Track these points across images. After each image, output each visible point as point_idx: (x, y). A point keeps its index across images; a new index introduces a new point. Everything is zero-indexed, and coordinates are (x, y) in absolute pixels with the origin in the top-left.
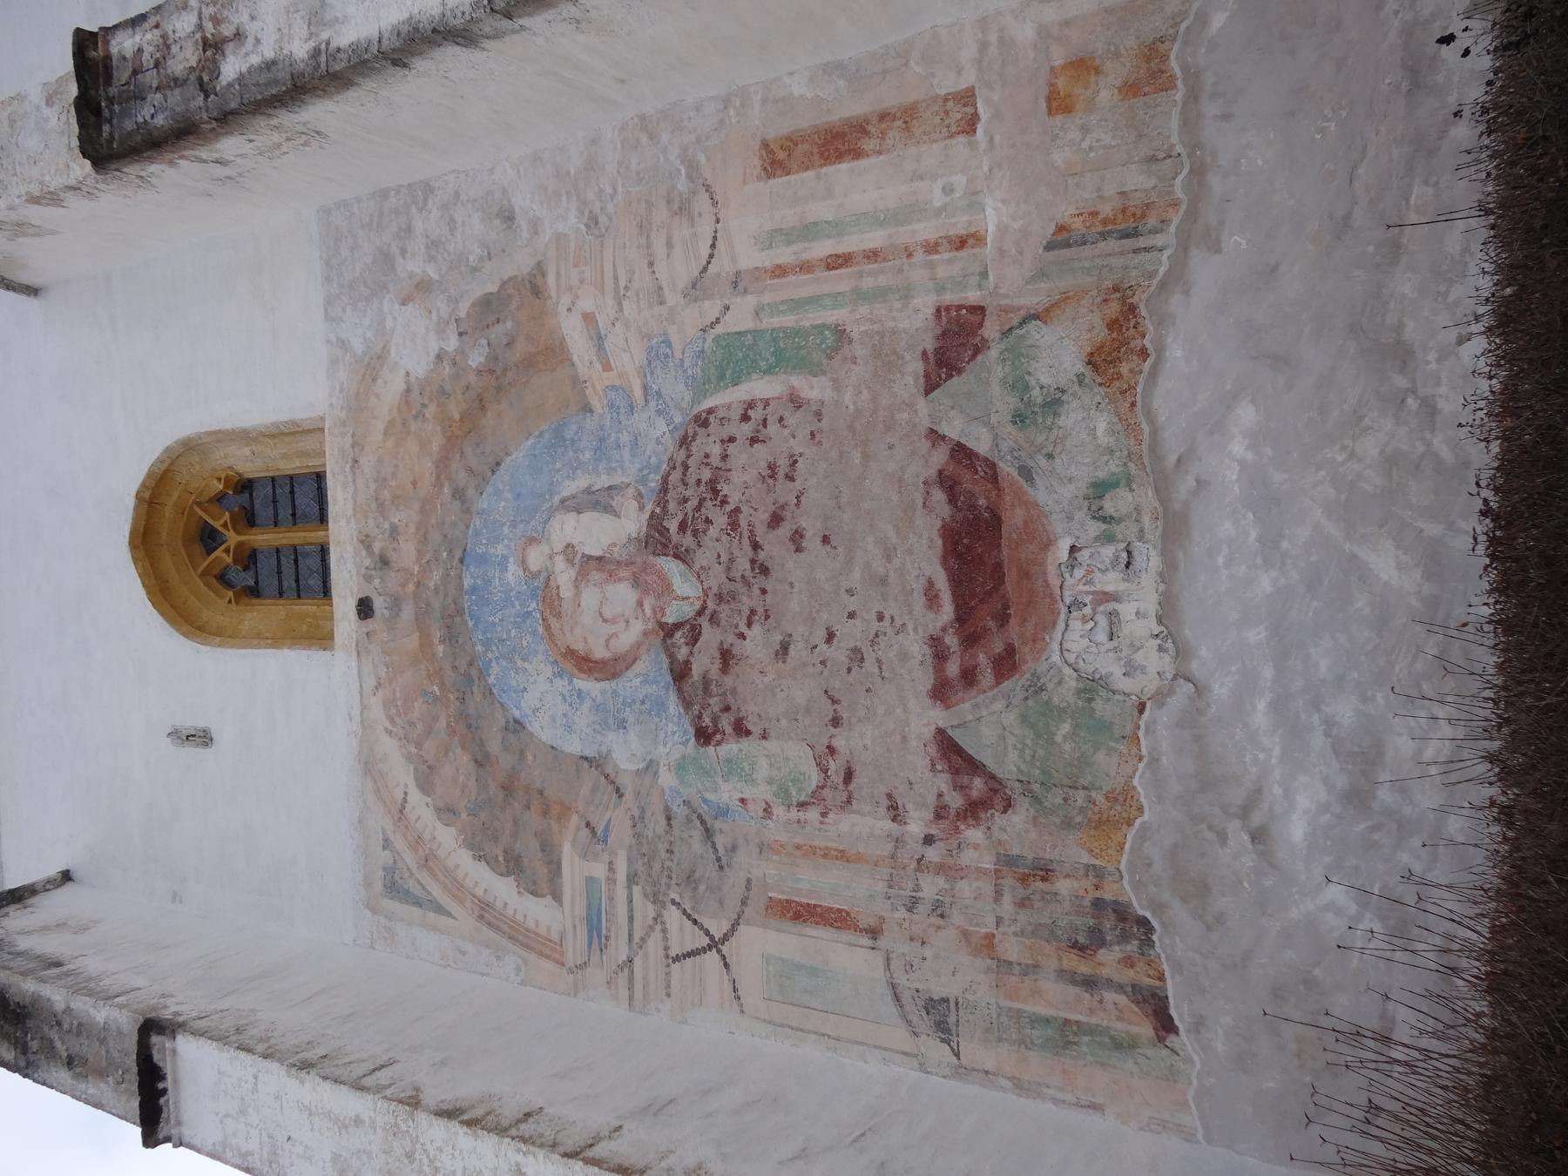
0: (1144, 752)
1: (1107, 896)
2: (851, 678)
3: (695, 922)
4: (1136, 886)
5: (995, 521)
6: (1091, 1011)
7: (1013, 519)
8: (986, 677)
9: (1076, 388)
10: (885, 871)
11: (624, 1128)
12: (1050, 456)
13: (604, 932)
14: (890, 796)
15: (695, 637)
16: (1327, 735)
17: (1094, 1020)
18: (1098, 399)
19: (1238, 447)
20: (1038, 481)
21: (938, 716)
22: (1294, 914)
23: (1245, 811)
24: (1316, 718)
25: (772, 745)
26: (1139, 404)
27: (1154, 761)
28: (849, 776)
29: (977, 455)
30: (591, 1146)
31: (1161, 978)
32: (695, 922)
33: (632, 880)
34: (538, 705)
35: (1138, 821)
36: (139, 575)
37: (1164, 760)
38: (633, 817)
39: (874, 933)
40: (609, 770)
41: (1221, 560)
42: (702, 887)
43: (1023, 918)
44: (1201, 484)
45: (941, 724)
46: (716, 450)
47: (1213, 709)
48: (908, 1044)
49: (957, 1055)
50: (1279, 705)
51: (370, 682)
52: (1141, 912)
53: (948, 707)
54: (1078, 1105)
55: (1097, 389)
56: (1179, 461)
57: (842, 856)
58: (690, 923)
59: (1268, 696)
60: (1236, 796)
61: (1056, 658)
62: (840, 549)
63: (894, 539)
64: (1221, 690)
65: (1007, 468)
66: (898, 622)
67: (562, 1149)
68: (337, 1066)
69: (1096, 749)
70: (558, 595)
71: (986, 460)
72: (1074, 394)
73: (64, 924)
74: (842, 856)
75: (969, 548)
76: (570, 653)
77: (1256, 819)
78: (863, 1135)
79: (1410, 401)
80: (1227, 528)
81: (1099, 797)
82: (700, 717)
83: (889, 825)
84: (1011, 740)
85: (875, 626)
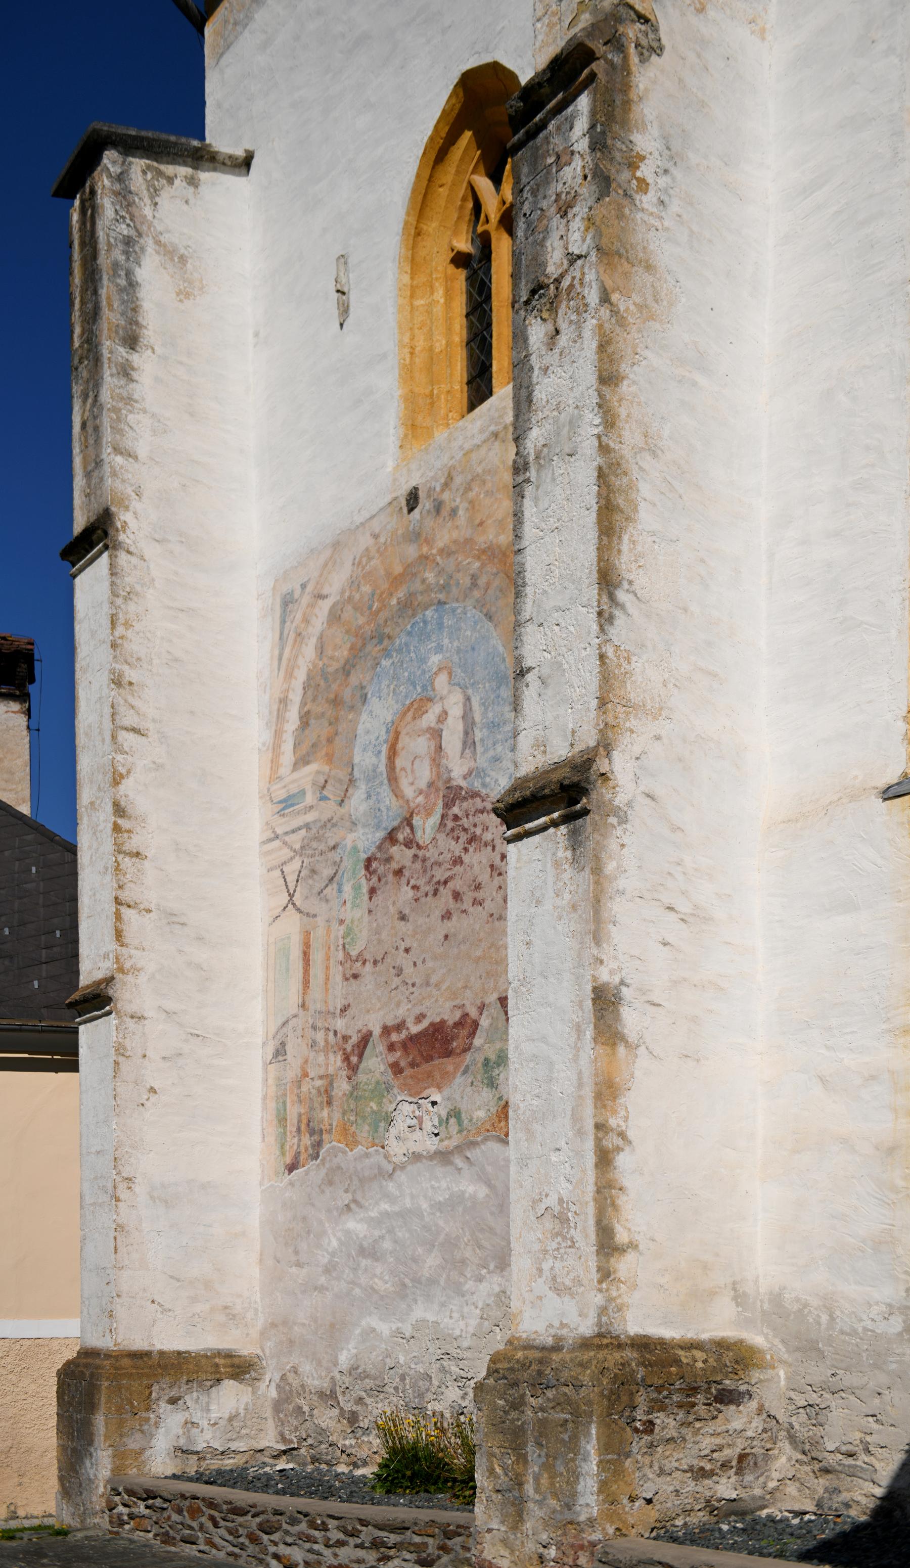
0: (370, 1150)
1: (324, 1136)
2: (391, 969)
3: (297, 881)
4: (327, 1151)
5: (448, 1053)
6: (291, 1132)
7: (449, 1064)
8: (391, 1059)
9: (497, 1096)
10: (324, 1009)
11: (151, 914)
12: (472, 1084)
13: (286, 811)
14: (349, 1005)
15: (408, 844)
16: (379, 1237)
17: (288, 1134)
18: (492, 1110)
19: (471, 1189)
20: (463, 1078)
21: (377, 1031)
22: (327, 1225)
23: (355, 1201)
24: (384, 1231)
25: (366, 918)
26: (488, 1134)
27: (367, 1155)
28: (355, 976)
29: (473, 1038)
30: (129, 906)
31: (303, 1166)
32: (297, 881)
33: (307, 826)
34: (374, 714)
35: (347, 1149)
36: (444, 110)
37: (367, 1160)
38: (332, 818)
39: (303, 1006)
40: (350, 791)
41: (433, 1183)
42: (310, 882)
43: (314, 1092)
44: (459, 1170)
45: (374, 1033)
46: (488, 836)
47: (385, 1183)
48: (270, 1036)
49: (270, 1063)
50: (386, 1214)
51: (376, 526)
52: (321, 1154)
53: (380, 1037)
54: (263, 1129)
55: (496, 1108)
56: (468, 1158)
57: (327, 979)
58: (296, 877)
59: (389, 1209)
60: (359, 1197)
61: (399, 1098)
62: (442, 949)
63: (444, 987)
64: (391, 1186)
65: (468, 1057)
66: (412, 997)
67: (120, 893)
68: (126, 701)
69: (369, 1125)
70: (422, 714)
71: (471, 1044)
72: (494, 1096)
73: (183, 259)
74: (327, 979)
75: (437, 1039)
76: (397, 734)
77: (353, 1206)
78: (198, 1036)
79: (485, 1271)
80: (444, 1184)
81: (353, 1129)
82: (376, 859)
83: (339, 1007)
84: (369, 1076)
85: (410, 982)
